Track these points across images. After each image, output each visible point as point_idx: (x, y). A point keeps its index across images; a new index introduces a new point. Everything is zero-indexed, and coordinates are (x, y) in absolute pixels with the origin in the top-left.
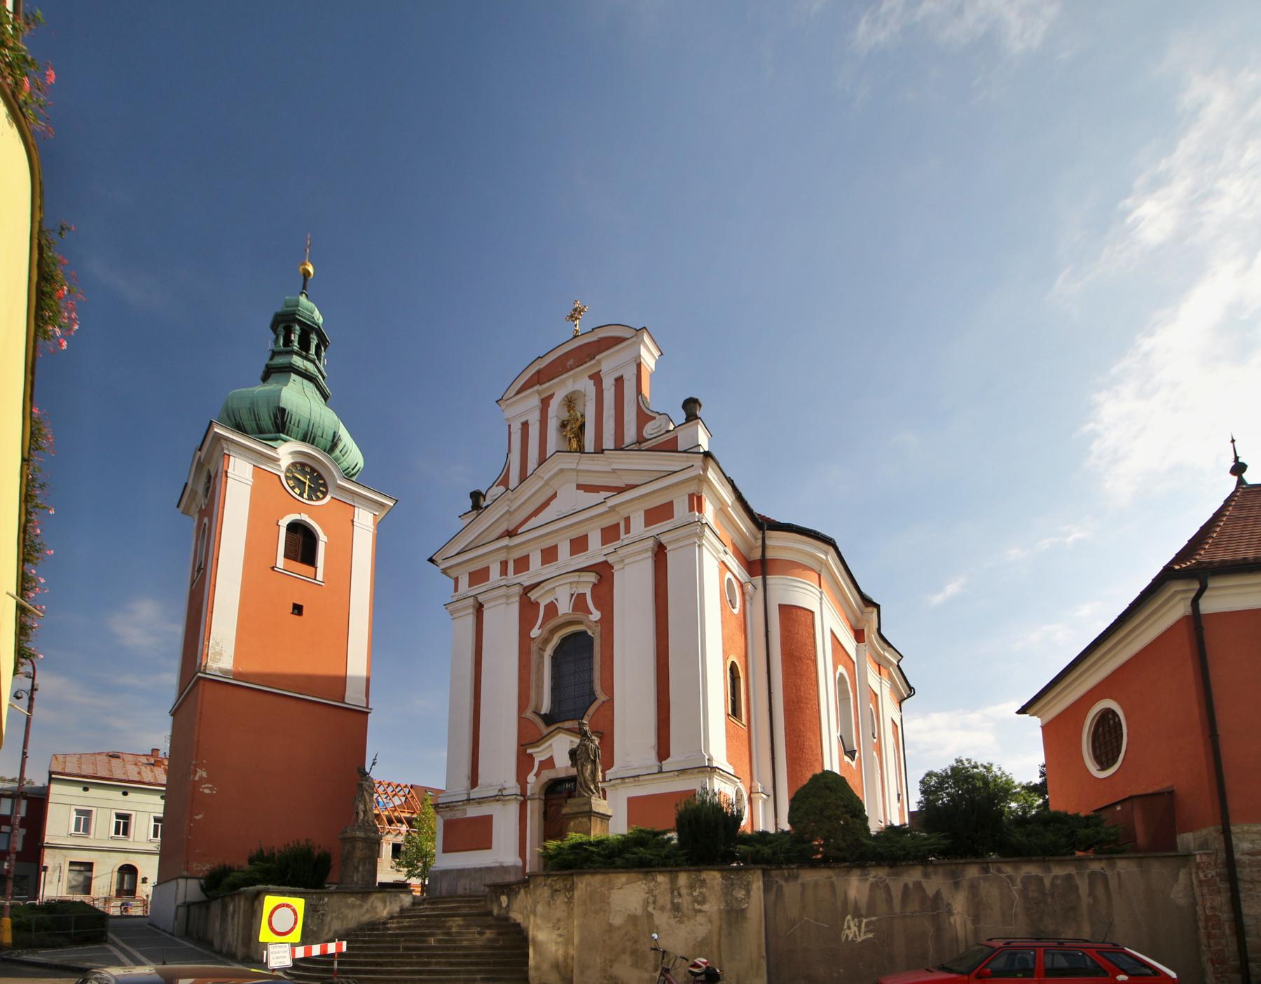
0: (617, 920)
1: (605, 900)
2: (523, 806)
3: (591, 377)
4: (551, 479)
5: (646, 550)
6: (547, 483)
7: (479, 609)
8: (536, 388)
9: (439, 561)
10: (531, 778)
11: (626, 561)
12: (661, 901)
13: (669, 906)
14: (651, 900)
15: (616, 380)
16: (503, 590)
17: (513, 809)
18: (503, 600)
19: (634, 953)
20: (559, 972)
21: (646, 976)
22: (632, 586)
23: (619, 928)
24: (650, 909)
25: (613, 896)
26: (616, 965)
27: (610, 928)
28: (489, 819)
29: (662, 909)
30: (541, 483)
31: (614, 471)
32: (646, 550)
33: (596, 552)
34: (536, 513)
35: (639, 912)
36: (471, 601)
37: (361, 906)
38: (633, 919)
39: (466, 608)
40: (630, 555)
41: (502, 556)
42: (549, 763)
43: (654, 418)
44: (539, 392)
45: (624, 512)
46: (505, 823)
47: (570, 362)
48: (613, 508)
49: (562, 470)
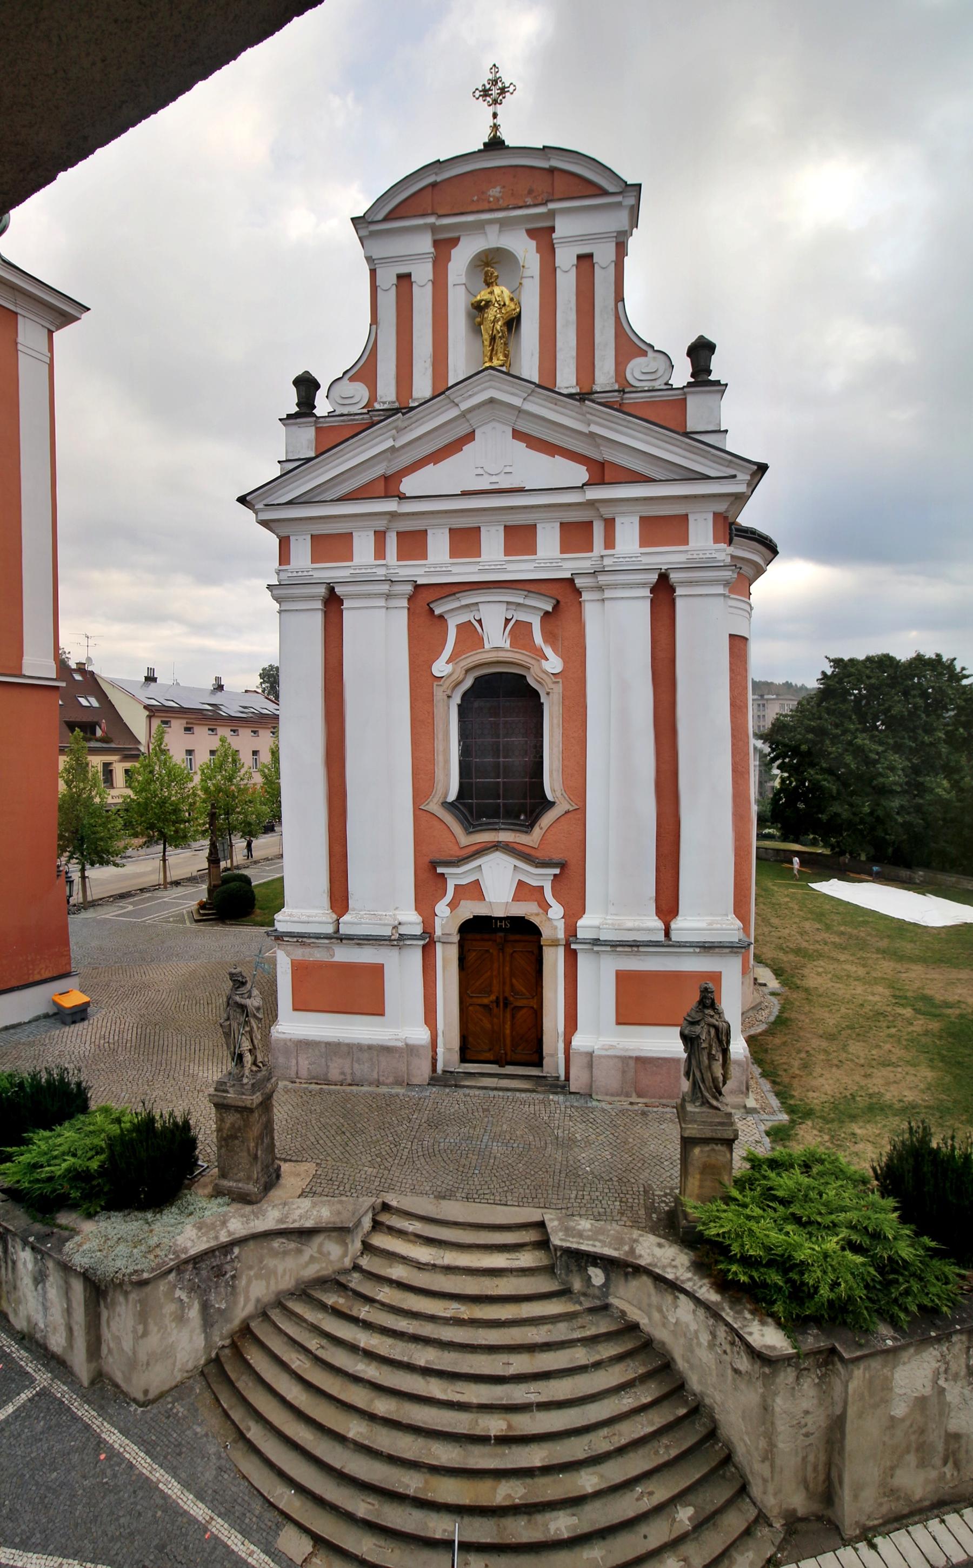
0: (900, 1410)
1: (887, 1386)
2: (428, 950)
3: (531, 233)
4: (470, 410)
5: (643, 585)
6: (463, 415)
7: (333, 602)
8: (431, 220)
9: (259, 506)
10: (442, 909)
11: (607, 594)
12: (954, 1367)
13: (963, 1372)
14: (942, 1369)
15: (580, 257)
16: (385, 588)
17: (415, 957)
18: (382, 602)
19: (920, 1448)
20: (807, 1488)
21: (934, 1474)
22: (616, 631)
23: (903, 1420)
24: (941, 1382)
25: (896, 1376)
26: (898, 1472)
27: (893, 1422)
28: (378, 970)
29: (956, 1377)
30: (454, 413)
31: (592, 435)
32: (643, 585)
33: (549, 557)
34: (436, 457)
35: (927, 1391)
36: (322, 590)
37: (299, 1251)
38: (921, 1402)
39: (312, 598)
40: (614, 586)
41: (381, 524)
42: (475, 890)
43: (644, 354)
44: (434, 229)
45: (607, 512)
46: (403, 975)
47: (495, 192)
48: (592, 503)
49: (492, 401)
